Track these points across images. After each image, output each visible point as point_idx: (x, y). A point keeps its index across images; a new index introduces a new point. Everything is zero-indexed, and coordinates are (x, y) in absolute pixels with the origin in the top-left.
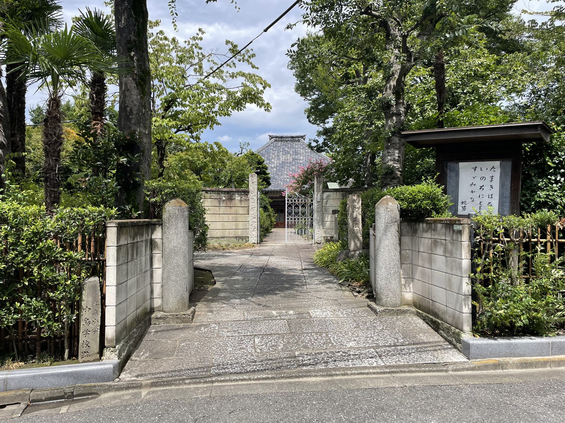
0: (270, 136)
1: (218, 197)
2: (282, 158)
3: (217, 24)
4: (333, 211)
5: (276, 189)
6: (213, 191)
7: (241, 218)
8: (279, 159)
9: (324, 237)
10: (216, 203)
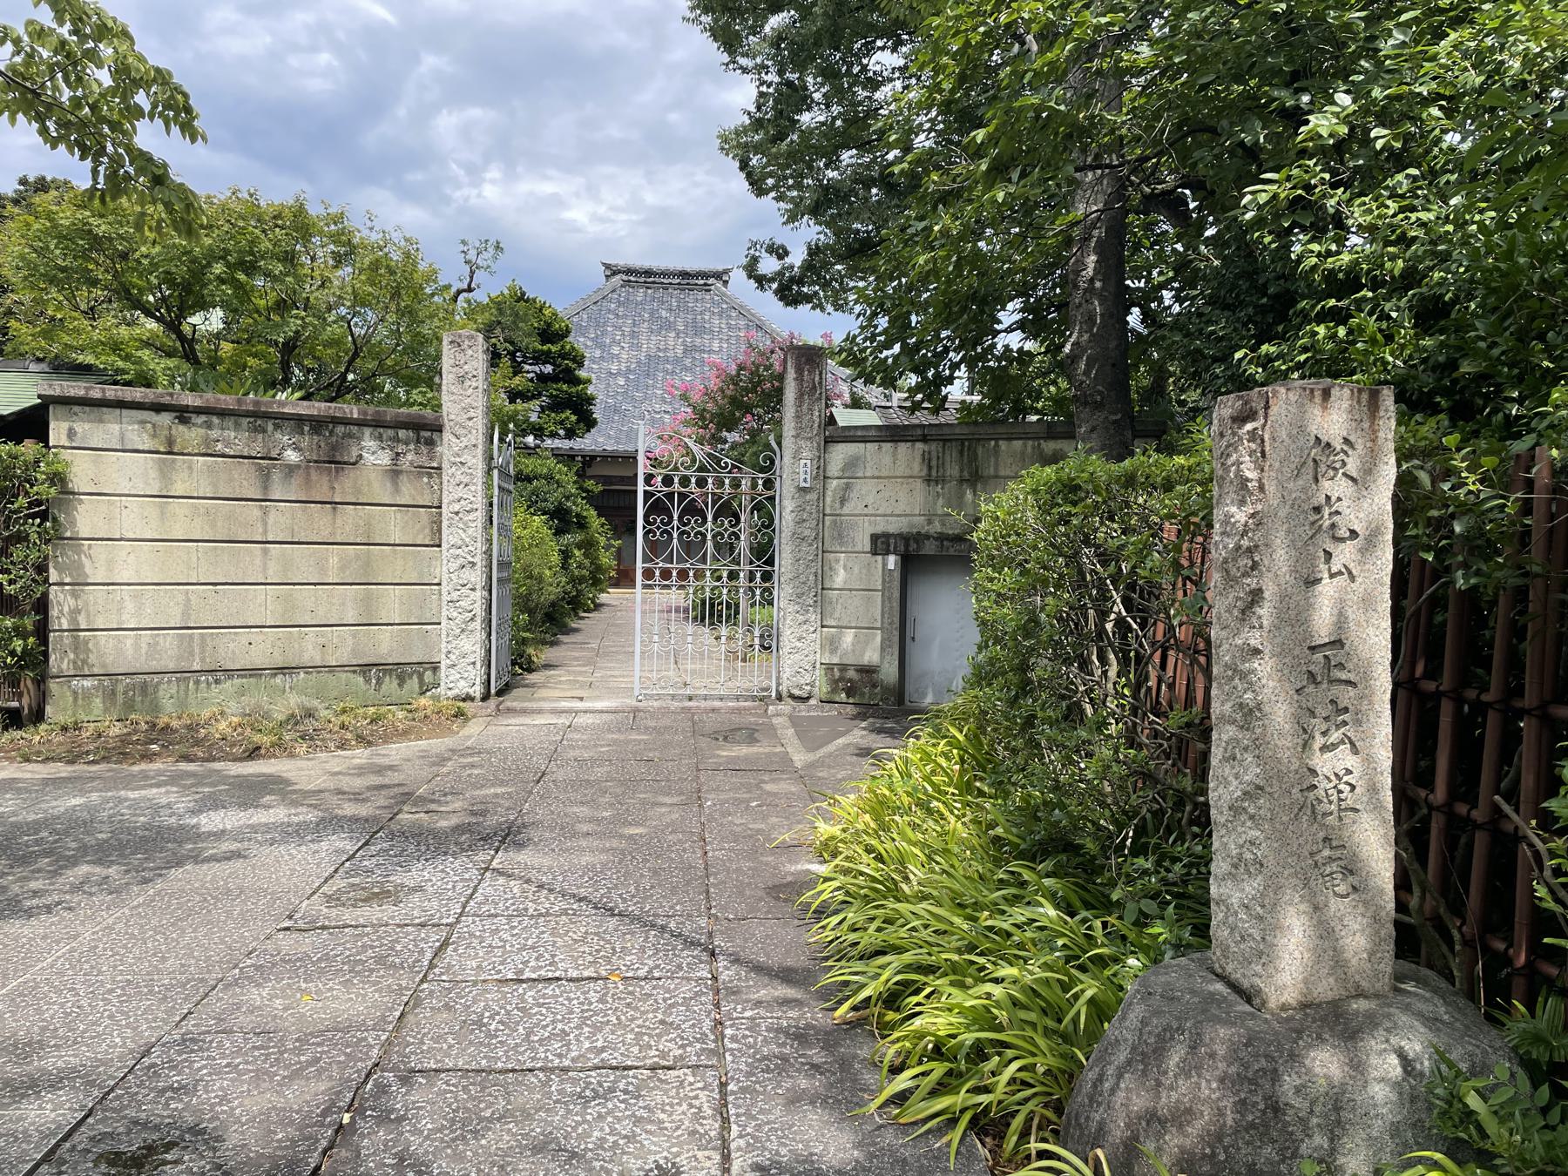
0: (607, 267)
1: (257, 448)
2: (649, 343)
4: (875, 538)
5: (621, 448)
6: (223, 413)
7: (395, 566)
8: (639, 347)
9: (829, 668)
10: (244, 480)
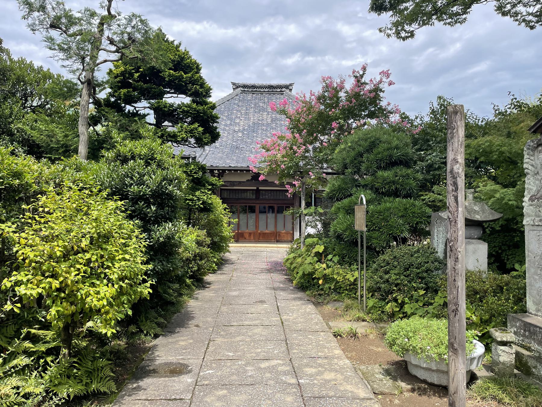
0: (234, 84)
2: (254, 118)
3: (205, 23)
8: (249, 119)
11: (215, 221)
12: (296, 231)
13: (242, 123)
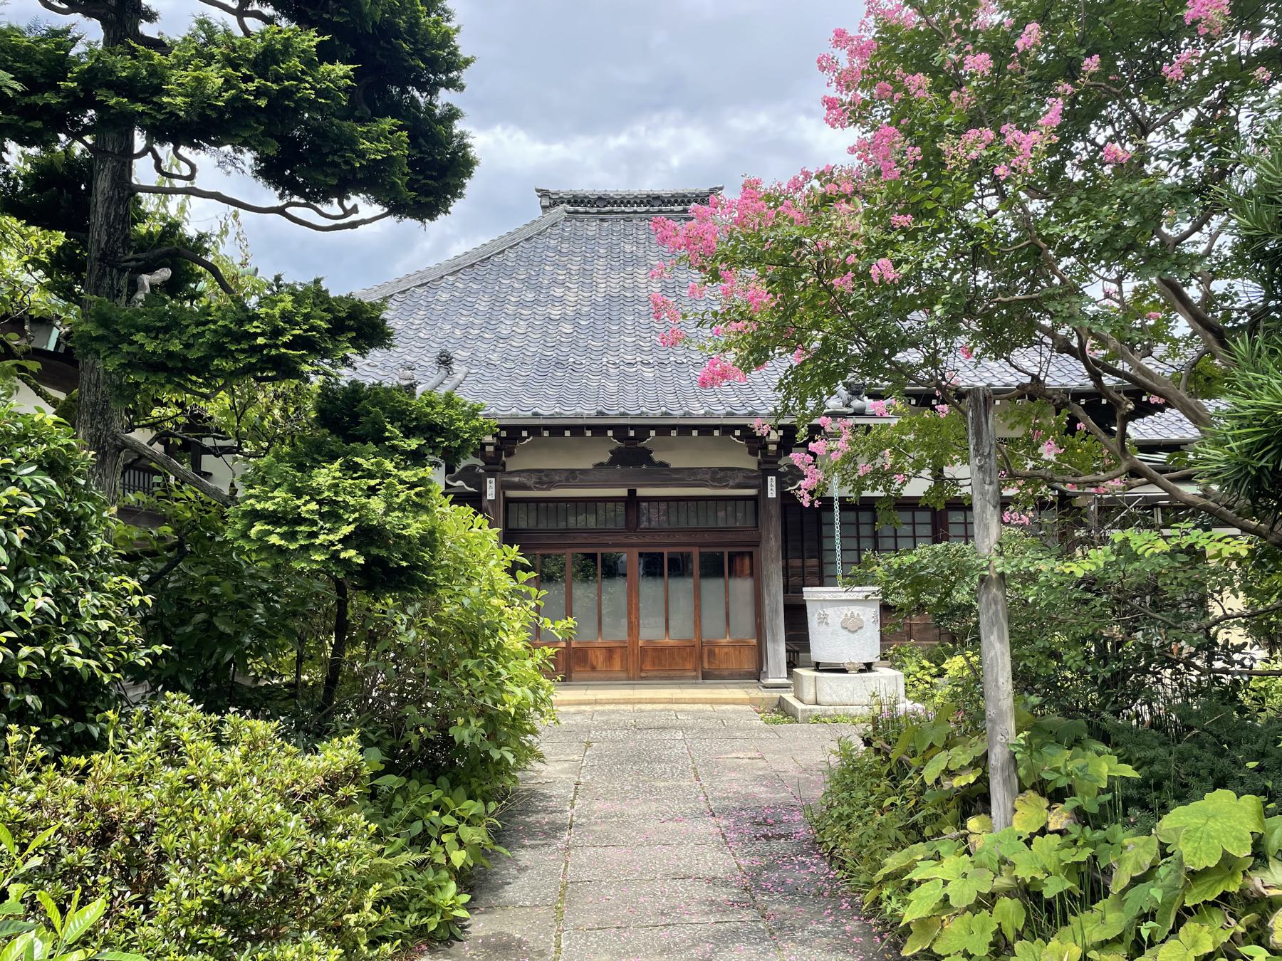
0: (543, 193)
2: (607, 282)
8: (593, 287)
11: (460, 629)
12: (775, 640)
13: (571, 298)
